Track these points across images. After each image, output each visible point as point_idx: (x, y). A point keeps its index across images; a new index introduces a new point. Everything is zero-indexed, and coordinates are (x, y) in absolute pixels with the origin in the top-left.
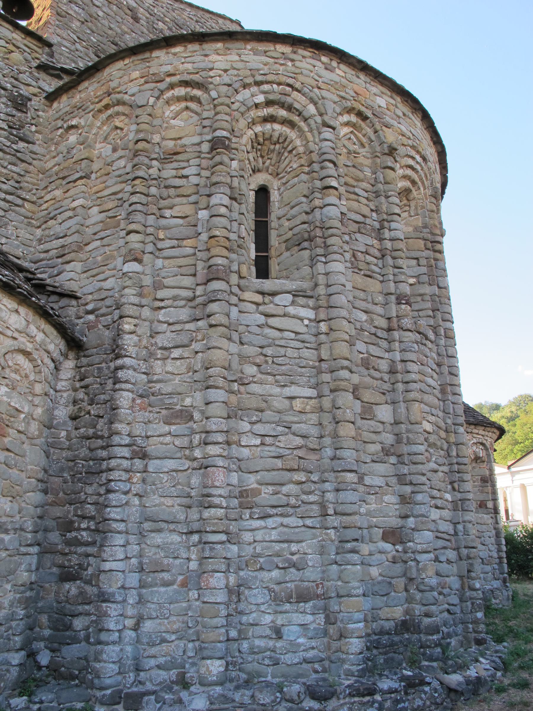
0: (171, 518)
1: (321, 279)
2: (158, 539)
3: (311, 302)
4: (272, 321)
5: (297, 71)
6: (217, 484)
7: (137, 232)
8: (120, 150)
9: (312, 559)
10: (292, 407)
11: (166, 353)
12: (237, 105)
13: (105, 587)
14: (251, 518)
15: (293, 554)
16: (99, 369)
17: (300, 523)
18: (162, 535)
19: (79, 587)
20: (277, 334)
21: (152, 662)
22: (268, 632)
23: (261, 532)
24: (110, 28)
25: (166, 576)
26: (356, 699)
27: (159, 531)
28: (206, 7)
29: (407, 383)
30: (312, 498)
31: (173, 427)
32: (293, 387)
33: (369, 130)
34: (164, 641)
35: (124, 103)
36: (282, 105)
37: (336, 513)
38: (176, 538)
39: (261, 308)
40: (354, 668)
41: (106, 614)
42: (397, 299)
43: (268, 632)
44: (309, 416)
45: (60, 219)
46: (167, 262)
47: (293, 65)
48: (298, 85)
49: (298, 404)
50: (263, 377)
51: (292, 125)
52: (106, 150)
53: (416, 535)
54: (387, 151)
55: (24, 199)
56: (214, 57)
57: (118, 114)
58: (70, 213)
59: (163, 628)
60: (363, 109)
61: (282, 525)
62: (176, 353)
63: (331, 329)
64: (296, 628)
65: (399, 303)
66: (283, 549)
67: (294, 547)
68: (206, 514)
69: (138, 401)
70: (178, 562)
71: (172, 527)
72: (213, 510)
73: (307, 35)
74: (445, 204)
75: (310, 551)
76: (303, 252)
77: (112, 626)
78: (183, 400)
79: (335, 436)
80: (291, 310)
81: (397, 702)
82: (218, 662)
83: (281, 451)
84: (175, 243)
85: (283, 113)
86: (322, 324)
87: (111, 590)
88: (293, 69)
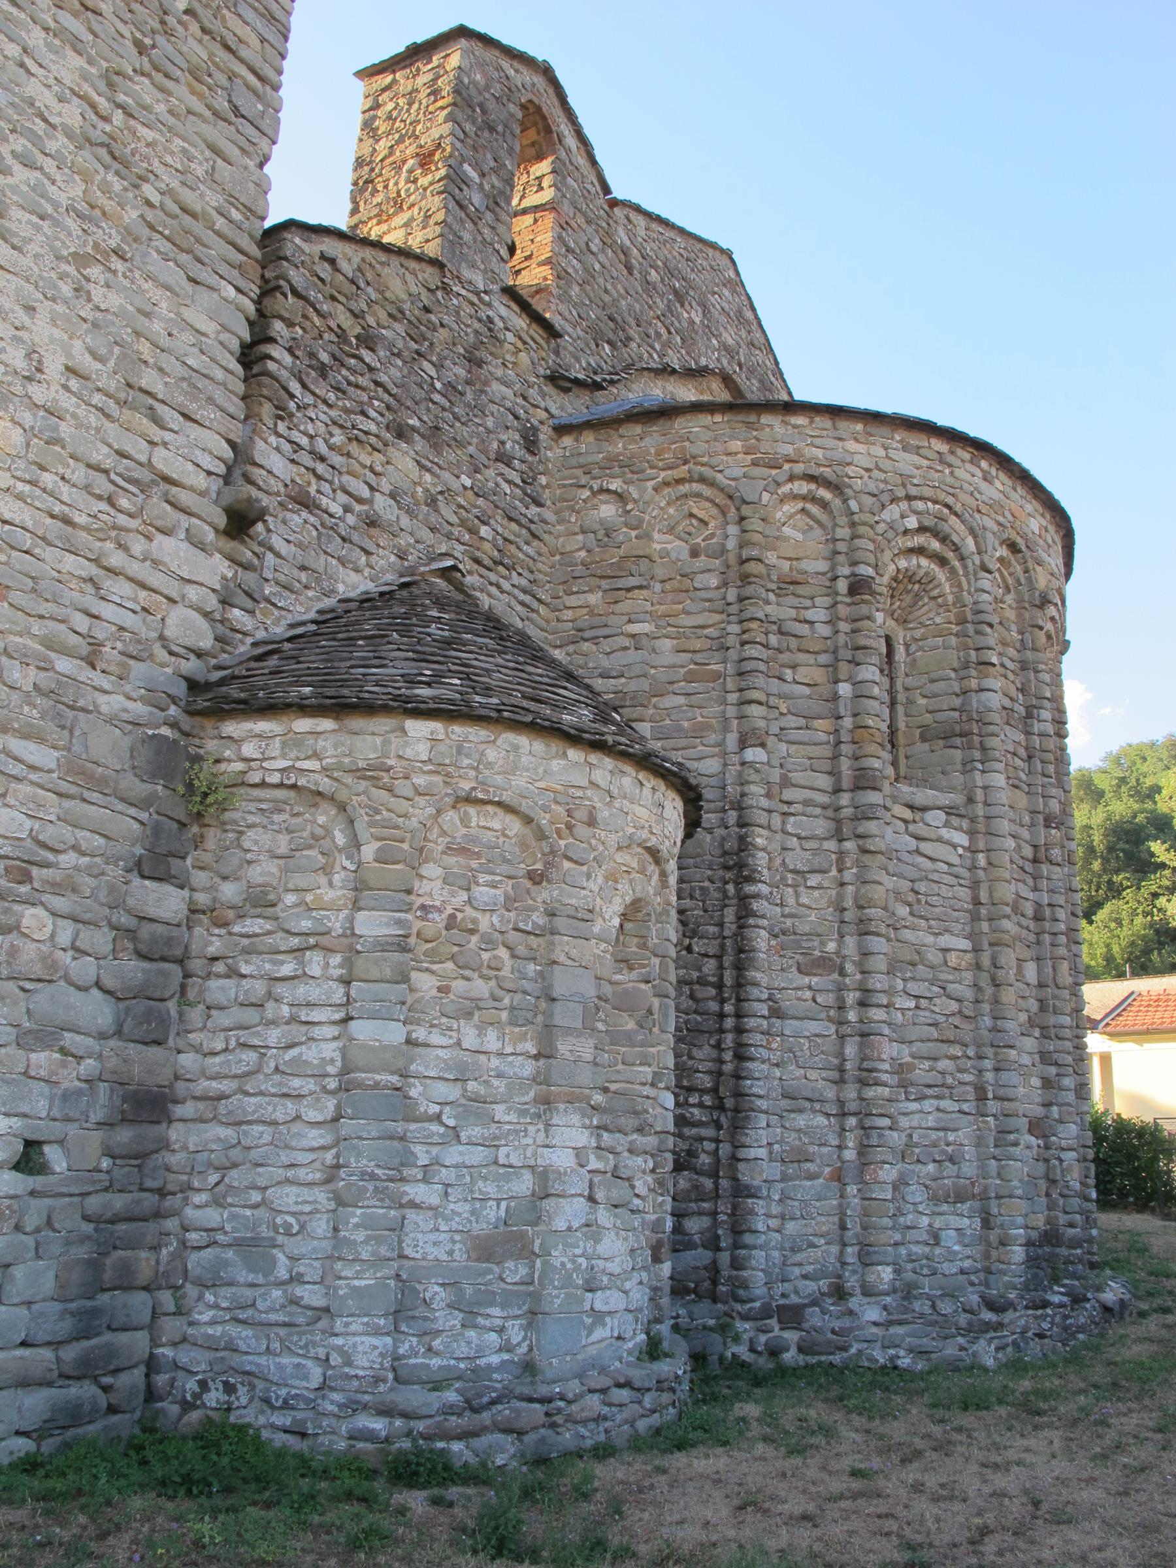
0: (816, 1096)
1: (979, 795)
2: (801, 1121)
3: (965, 824)
4: (926, 847)
5: (957, 484)
6: (884, 1057)
7: (760, 703)
8: (703, 558)
9: (969, 1151)
10: (946, 962)
11: (799, 878)
12: (881, 527)
13: (745, 1179)
14: (907, 1099)
15: (948, 1145)
16: (702, 888)
17: (955, 1107)
18: (805, 1116)
19: (690, 1180)
20: (928, 864)
21: (797, 1271)
22: (925, 1237)
23: (917, 1116)
24: (606, 291)
25: (811, 1167)
26: (1030, 1312)
27: (801, 1111)
28: (588, 131)
29: (1055, 934)
30: (967, 1078)
31: (815, 980)
32: (947, 937)
33: (1018, 568)
34: (812, 1245)
35: (712, 484)
36: (936, 534)
37: (995, 1098)
38: (822, 1120)
39: (911, 827)
40: (1017, 1280)
41: (752, 1212)
42: (1045, 820)
43: (925, 1237)
44: (964, 974)
45: (606, 645)
46: (793, 748)
47: (952, 473)
48: (958, 508)
49: (953, 959)
50: (916, 920)
51: (942, 561)
52: (678, 548)
53: (1060, 1128)
54: (1037, 602)
55: (540, 601)
56: (852, 445)
57: (698, 495)
58: (627, 642)
59: (810, 1231)
60: (1019, 540)
61: (938, 1109)
62: (813, 880)
63: (990, 864)
64: (952, 1233)
65: (1047, 826)
66: (939, 1138)
67: (951, 1137)
68: (870, 1093)
69: (773, 943)
70: (825, 1150)
71: (817, 1106)
72: (880, 1089)
73: (972, 433)
74: (1065, 658)
75: (966, 1142)
76: (952, 751)
77: (761, 1227)
78: (823, 944)
79: (996, 1001)
80: (945, 833)
81: (1066, 1317)
82: (889, 1269)
83: (938, 1017)
84: (802, 722)
85: (935, 545)
86: (981, 855)
87: (755, 1183)
88: (949, 480)
